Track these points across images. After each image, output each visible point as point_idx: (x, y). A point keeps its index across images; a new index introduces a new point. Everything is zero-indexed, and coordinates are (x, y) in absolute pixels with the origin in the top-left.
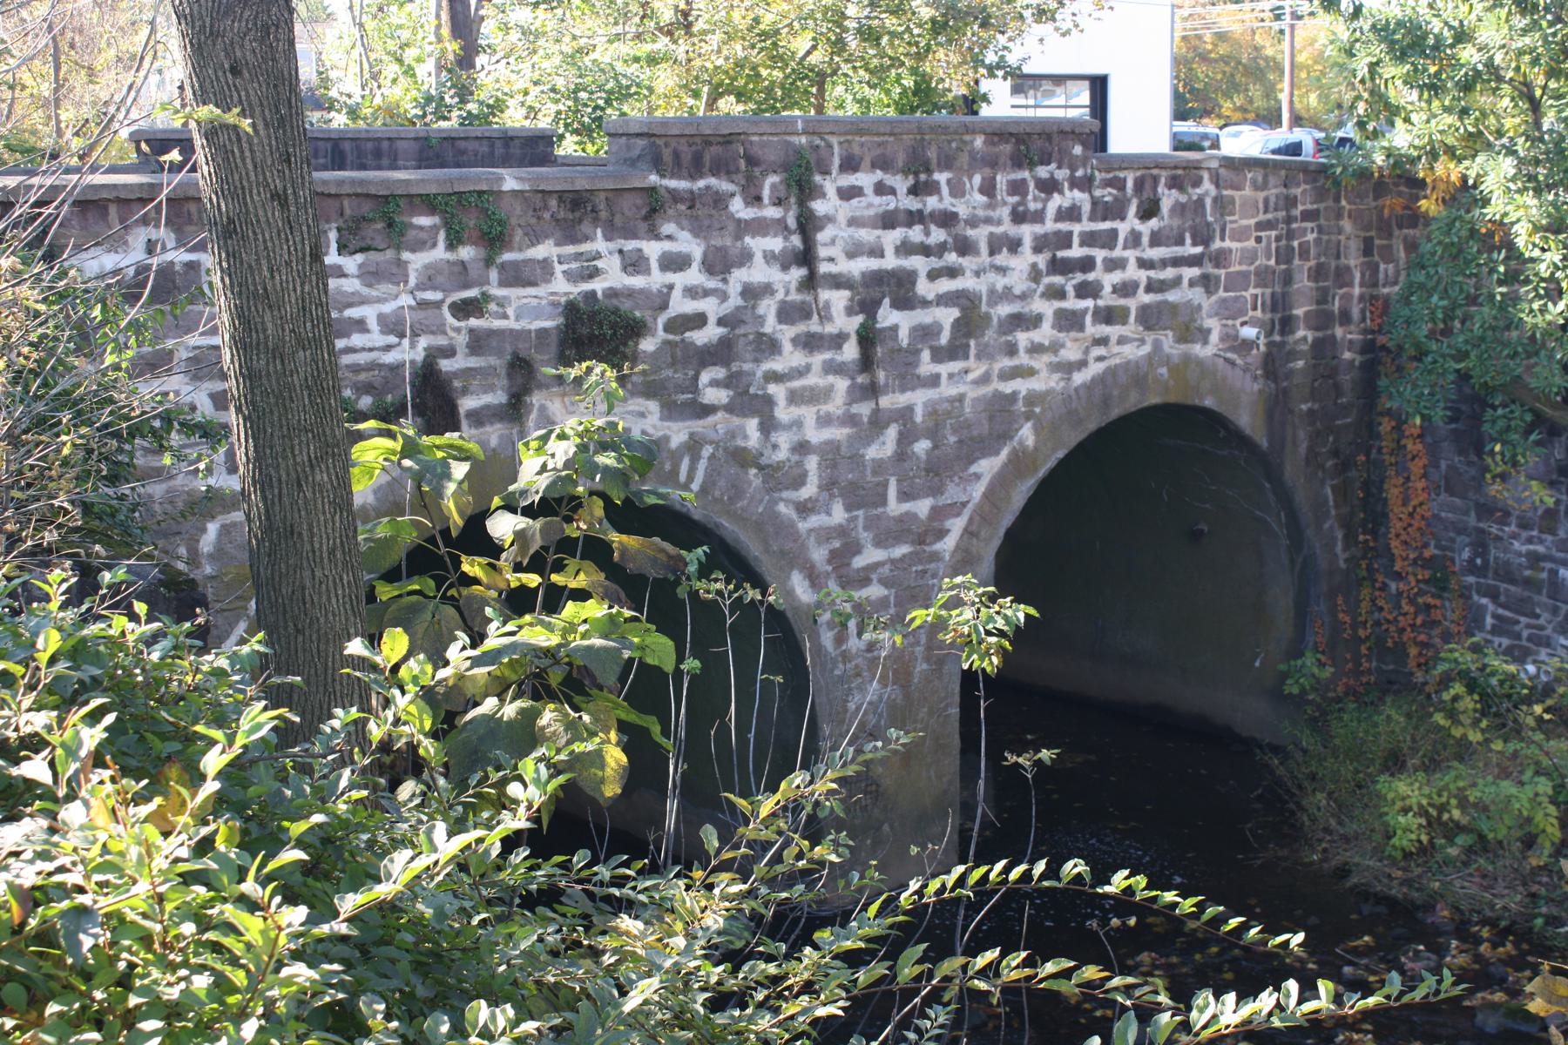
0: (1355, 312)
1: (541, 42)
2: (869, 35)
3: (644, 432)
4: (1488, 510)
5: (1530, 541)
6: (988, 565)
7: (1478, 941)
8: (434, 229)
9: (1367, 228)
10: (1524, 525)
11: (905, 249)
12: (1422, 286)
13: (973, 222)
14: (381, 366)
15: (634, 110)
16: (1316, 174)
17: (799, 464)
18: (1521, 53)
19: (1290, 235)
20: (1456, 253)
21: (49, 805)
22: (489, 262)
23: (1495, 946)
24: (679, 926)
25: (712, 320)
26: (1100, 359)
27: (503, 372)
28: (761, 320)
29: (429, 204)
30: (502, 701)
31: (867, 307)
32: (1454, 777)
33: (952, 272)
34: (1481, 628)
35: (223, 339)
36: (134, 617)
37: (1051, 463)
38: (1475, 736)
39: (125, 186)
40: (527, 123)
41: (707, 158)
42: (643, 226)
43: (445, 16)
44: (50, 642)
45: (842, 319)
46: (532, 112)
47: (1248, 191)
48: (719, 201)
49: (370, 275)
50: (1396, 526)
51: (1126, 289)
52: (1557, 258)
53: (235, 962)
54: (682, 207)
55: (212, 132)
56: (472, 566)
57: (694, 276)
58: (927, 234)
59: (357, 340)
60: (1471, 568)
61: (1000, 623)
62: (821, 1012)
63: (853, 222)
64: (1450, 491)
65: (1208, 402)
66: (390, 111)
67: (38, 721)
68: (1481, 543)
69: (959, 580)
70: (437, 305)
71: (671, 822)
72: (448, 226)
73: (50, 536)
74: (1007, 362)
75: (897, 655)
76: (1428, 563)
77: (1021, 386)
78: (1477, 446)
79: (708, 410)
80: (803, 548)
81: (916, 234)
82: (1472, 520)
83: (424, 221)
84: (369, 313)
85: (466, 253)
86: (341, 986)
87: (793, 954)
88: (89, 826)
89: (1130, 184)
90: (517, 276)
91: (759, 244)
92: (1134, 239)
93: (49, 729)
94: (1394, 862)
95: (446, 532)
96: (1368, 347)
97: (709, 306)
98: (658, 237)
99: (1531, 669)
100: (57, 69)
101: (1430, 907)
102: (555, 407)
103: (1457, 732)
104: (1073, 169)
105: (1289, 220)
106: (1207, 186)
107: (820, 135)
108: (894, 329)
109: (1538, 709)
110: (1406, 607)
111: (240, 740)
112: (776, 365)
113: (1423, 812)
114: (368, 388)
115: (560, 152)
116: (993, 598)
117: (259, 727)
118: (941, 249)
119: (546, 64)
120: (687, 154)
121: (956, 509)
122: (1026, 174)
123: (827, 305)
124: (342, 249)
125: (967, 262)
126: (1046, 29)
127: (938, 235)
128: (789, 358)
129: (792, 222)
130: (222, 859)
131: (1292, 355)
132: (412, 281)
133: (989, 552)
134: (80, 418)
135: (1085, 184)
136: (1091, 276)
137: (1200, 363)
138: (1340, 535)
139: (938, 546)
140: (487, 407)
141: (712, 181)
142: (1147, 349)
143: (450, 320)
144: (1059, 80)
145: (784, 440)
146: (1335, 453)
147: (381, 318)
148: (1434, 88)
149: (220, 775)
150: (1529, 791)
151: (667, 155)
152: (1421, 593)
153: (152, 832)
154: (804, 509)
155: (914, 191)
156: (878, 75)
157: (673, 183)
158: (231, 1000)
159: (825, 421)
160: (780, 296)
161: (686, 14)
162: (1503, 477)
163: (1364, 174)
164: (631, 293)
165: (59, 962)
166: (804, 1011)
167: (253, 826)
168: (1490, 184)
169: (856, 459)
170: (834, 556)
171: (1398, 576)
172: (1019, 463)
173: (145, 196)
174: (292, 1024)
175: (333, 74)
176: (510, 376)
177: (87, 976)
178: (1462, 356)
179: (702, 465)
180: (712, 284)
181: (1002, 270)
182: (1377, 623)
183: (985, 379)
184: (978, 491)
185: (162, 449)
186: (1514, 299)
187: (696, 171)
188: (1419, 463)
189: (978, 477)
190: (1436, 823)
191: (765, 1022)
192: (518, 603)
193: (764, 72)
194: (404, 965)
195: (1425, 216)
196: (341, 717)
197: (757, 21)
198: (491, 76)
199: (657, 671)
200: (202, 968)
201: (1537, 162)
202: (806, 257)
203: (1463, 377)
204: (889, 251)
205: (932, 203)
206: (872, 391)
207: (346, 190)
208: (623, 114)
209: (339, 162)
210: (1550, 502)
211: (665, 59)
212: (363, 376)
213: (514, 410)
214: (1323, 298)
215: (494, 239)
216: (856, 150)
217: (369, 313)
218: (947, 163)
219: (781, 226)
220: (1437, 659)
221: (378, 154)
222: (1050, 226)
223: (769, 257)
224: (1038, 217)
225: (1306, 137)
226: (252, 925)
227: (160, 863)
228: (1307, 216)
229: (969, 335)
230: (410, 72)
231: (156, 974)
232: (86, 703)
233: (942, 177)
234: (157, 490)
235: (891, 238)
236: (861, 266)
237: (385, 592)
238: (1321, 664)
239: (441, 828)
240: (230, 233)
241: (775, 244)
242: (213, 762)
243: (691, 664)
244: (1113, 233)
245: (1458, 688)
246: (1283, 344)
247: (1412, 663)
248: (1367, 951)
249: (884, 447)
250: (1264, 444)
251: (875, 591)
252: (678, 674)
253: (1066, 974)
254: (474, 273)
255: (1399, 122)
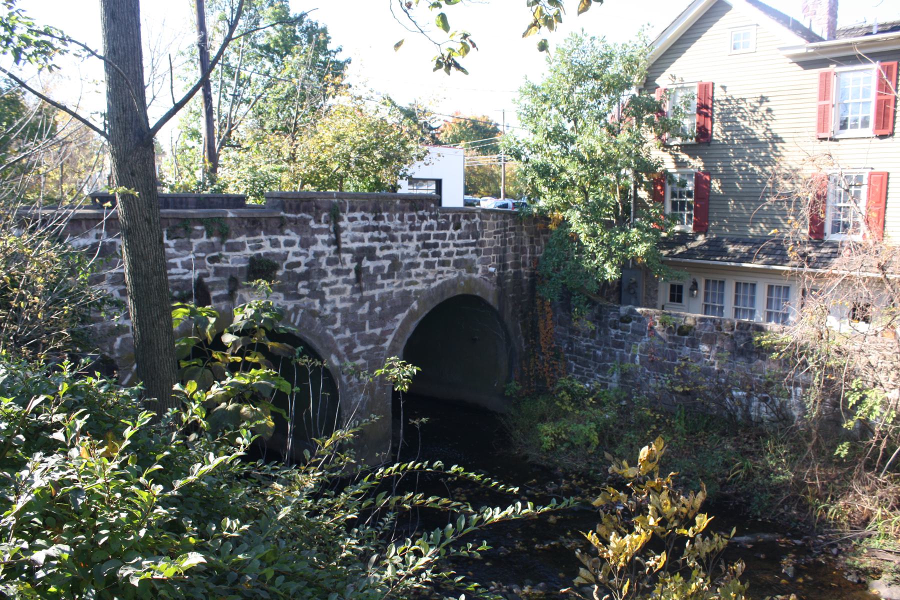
0: (528, 263)
1: (241, 164)
2: (359, 163)
3: (278, 305)
4: (573, 331)
5: (587, 341)
6: (401, 352)
7: (571, 479)
8: (202, 231)
9: (531, 234)
10: (585, 336)
11: (372, 239)
12: (550, 254)
13: (396, 230)
14: (182, 280)
15: (275, 189)
16: (513, 215)
17: (334, 316)
18: (581, 177)
19: (506, 236)
20: (561, 243)
21: (64, 449)
22: (222, 243)
23: (577, 481)
24: (297, 487)
25: (303, 264)
26: (440, 278)
27: (227, 283)
28: (320, 264)
29: (200, 222)
30: (228, 404)
31: (358, 259)
32: (563, 423)
33: (389, 248)
34: (571, 371)
35: (126, 270)
36: (96, 378)
37: (423, 315)
38: (570, 409)
39: (88, 214)
40: (235, 192)
41: (301, 206)
42: (278, 230)
43: (206, 154)
44: (64, 387)
45: (350, 265)
46: (238, 189)
47: (491, 221)
48: (306, 222)
49: (178, 247)
50: (542, 336)
51: (449, 254)
52: (594, 245)
53: (136, 507)
54: (292, 224)
55: (123, 196)
56: (216, 355)
57: (296, 248)
58: (380, 234)
59: (173, 271)
60: (567, 351)
61: (408, 373)
62: (349, 517)
63: (354, 230)
64: (560, 324)
65: (478, 294)
66: (186, 187)
67: (59, 417)
68: (571, 342)
69: (392, 358)
70: (203, 258)
71: (289, 446)
72: (207, 229)
73: (59, 345)
74: (408, 280)
75: (370, 384)
76: (553, 349)
77: (413, 288)
78: (568, 308)
79: (301, 296)
80: (335, 346)
81: (376, 234)
82: (568, 334)
83: (199, 228)
84: (178, 261)
85: (214, 239)
86: (176, 515)
87: (337, 495)
88: (80, 457)
89: (451, 218)
90: (232, 248)
91: (320, 237)
92: (452, 237)
93: (64, 420)
94: (543, 453)
95: (206, 340)
96: (532, 275)
97: (302, 259)
98: (283, 234)
99: (588, 385)
100: (62, 170)
101: (555, 469)
102: (246, 295)
103: (564, 408)
104: (431, 212)
105: (505, 231)
106: (477, 219)
107: (342, 199)
108: (368, 267)
109: (591, 399)
110: (546, 365)
111: (138, 425)
112: (326, 280)
113: (553, 436)
114: (177, 288)
115: (248, 203)
116: (405, 365)
117: (145, 420)
118: (385, 240)
119: (242, 171)
120: (294, 204)
121: (390, 332)
122: (414, 214)
123: (344, 259)
124: (169, 238)
125: (394, 244)
126: (421, 163)
127: (384, 235)
128: (331, 278)
129: (331, 229)
130: (131, 469)
131: (507, 277)
132: (194, 249)
133: (401, 346)
134: (72, 301)
135: (435, 217)
136: (437, 250)
137: (475, 280)
138: (523, 340)
139: (384, 345)
140: (221, 295)
141: (303, 214)
142: (457, 275)
143: (208, 263)
144: (425, 180)
145: (328, 307)
146: (521, 311)
147: (182, 263)
148: (553, 187)
149: (130, 439)
150: (588, 427)
151: (287, 205)
152: (551, 360)
153: (105, 460)
154: (336, 332)
155: (375, 219)
156: (362, 177)
157: (289, 215)
158: (135, 522)
159: (343, 300)
160: (327, 256)
161: (293, 155)
162: (578, 319)
163: (530, 216)
164: (273, 254)
165: (69, 509)
166: (343, 517)
167: (140, 454)
168: (572, 220)
169: (354, 314)
170: (346, 349)
171: (543, 354)
172: (412, 315)
173: (98, 218)
174: (157, 529)
175: (165, 174)
176: (229, 284)
177: (78, 514)
178: (564, 278)
179: (299, 316)
180: (303, 251)
181: (406, 247)
182: (536, 370)
183: (400, 286)
184: (398, 325)
185: (100, 311)
186: (580, 259)
187: (297, 211)
188: (550, 315)
189: (397, 320)
190: (557, 439)
191: (329, 521)
192: (233, 368)
193: (321, 176)
194: (197, 504)
195: (551, 230)
196: (170, 412)
197: (319, 158)
198: (222, 174)
199: (285, 395)
200: (122, 511)
201: (587, 213)
202: (337, 242)
203: (564, 285)
204: (366, 240)
205: (381, 223)
206: (360, 290)
207: (170, 216)
208: (270, 190)
209: (167, 206)
210: (593, 328)
211: (286, 170)
212: (175, 284)
213: (231, 297)
214: (517, 258)
215: (224, 235)
216: (355, 204)
217: (178, 261)
218: (387, 209)
219: (327, 231)
220: (556, 382)
221: (181, 203)
222: (423, 232)
223: (324, 242)
224: (419, 229)
225: (509, 202)
226: (144, 495)
227: (108, 471)
228: (511, 229)
229: (394, 270)
230: (192, 173)
231: (106, 512)
232: (78, 410)
233: (385, 214)
234: (98, 326)
235: (367, 235)
236: (356, 245)
237: (184, 364)
238: (517, 385)
239: (212, 454)
240: (129, 233)
241: (326, 237)
242: (128, 433)
243: (297, 389)
244: (445, 234)
245: (564, 393)
246: (503, 274)
247: (548, 384)
248: (534, 485)
249: (364, 310)
250: (497, 308)
251: (360, 362)
252: (292, 392)
253: (436, 502)
254: (216, 247)
255: (542, 198)
